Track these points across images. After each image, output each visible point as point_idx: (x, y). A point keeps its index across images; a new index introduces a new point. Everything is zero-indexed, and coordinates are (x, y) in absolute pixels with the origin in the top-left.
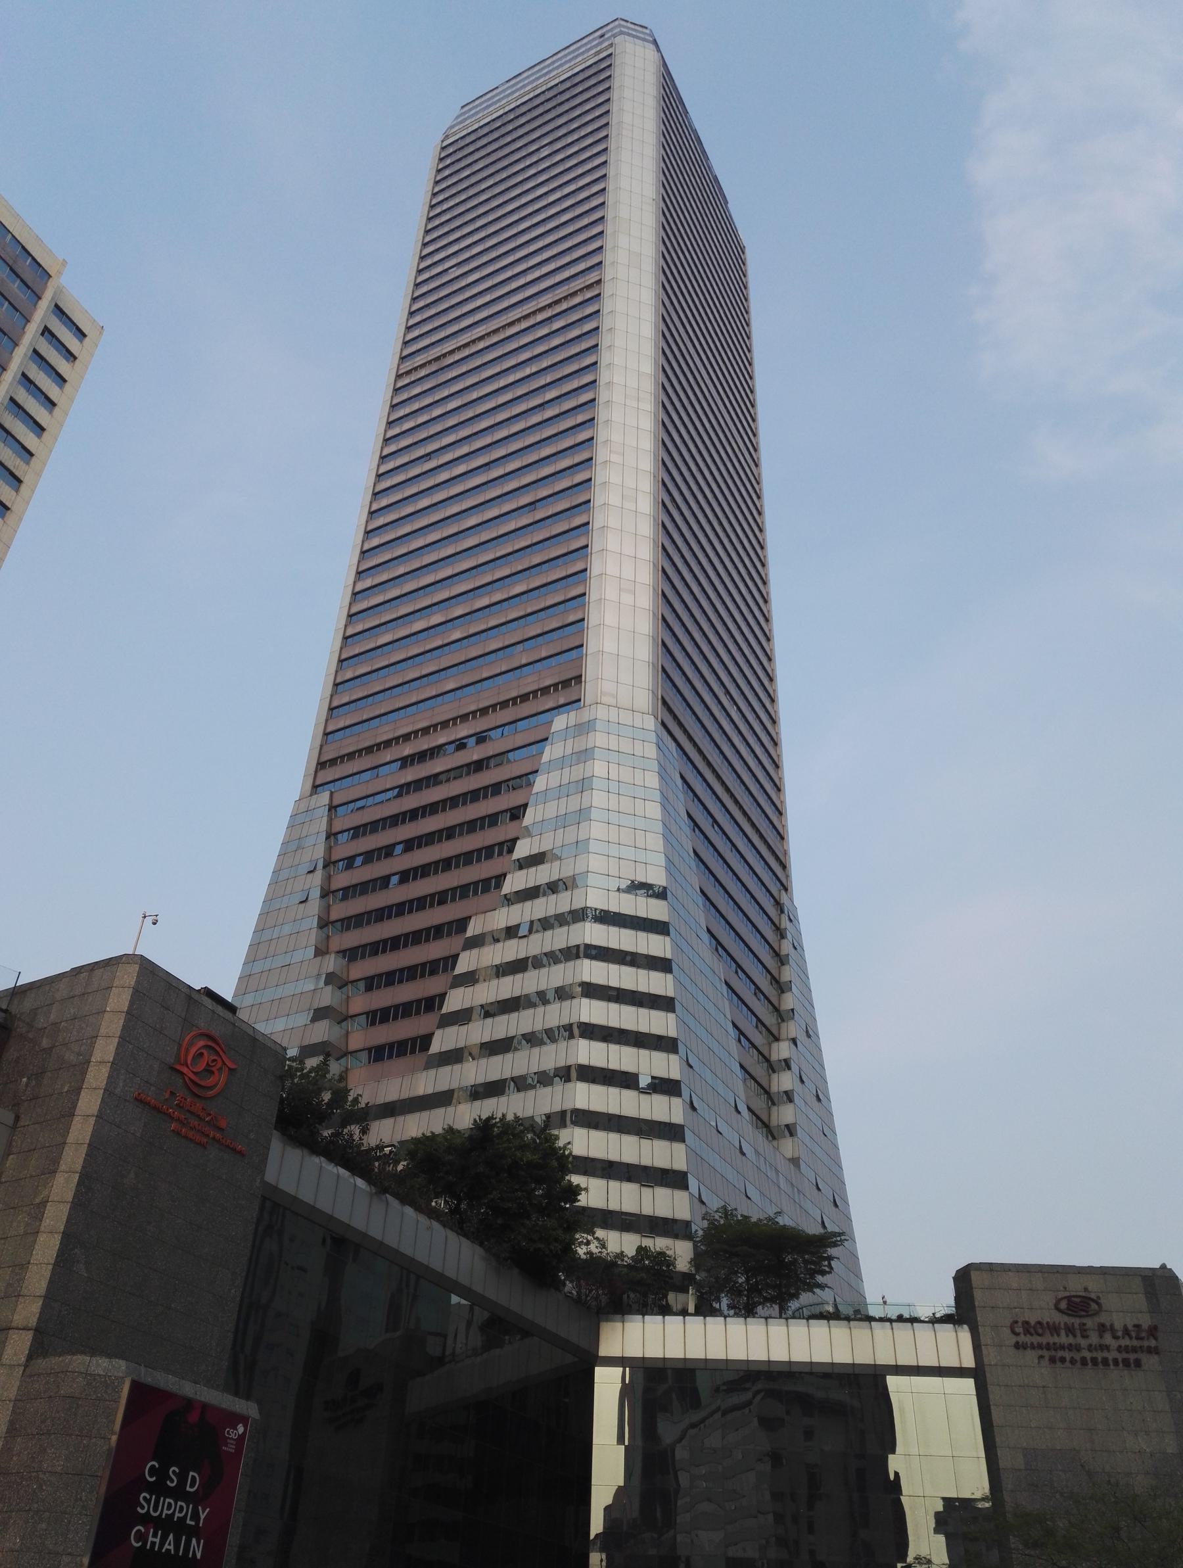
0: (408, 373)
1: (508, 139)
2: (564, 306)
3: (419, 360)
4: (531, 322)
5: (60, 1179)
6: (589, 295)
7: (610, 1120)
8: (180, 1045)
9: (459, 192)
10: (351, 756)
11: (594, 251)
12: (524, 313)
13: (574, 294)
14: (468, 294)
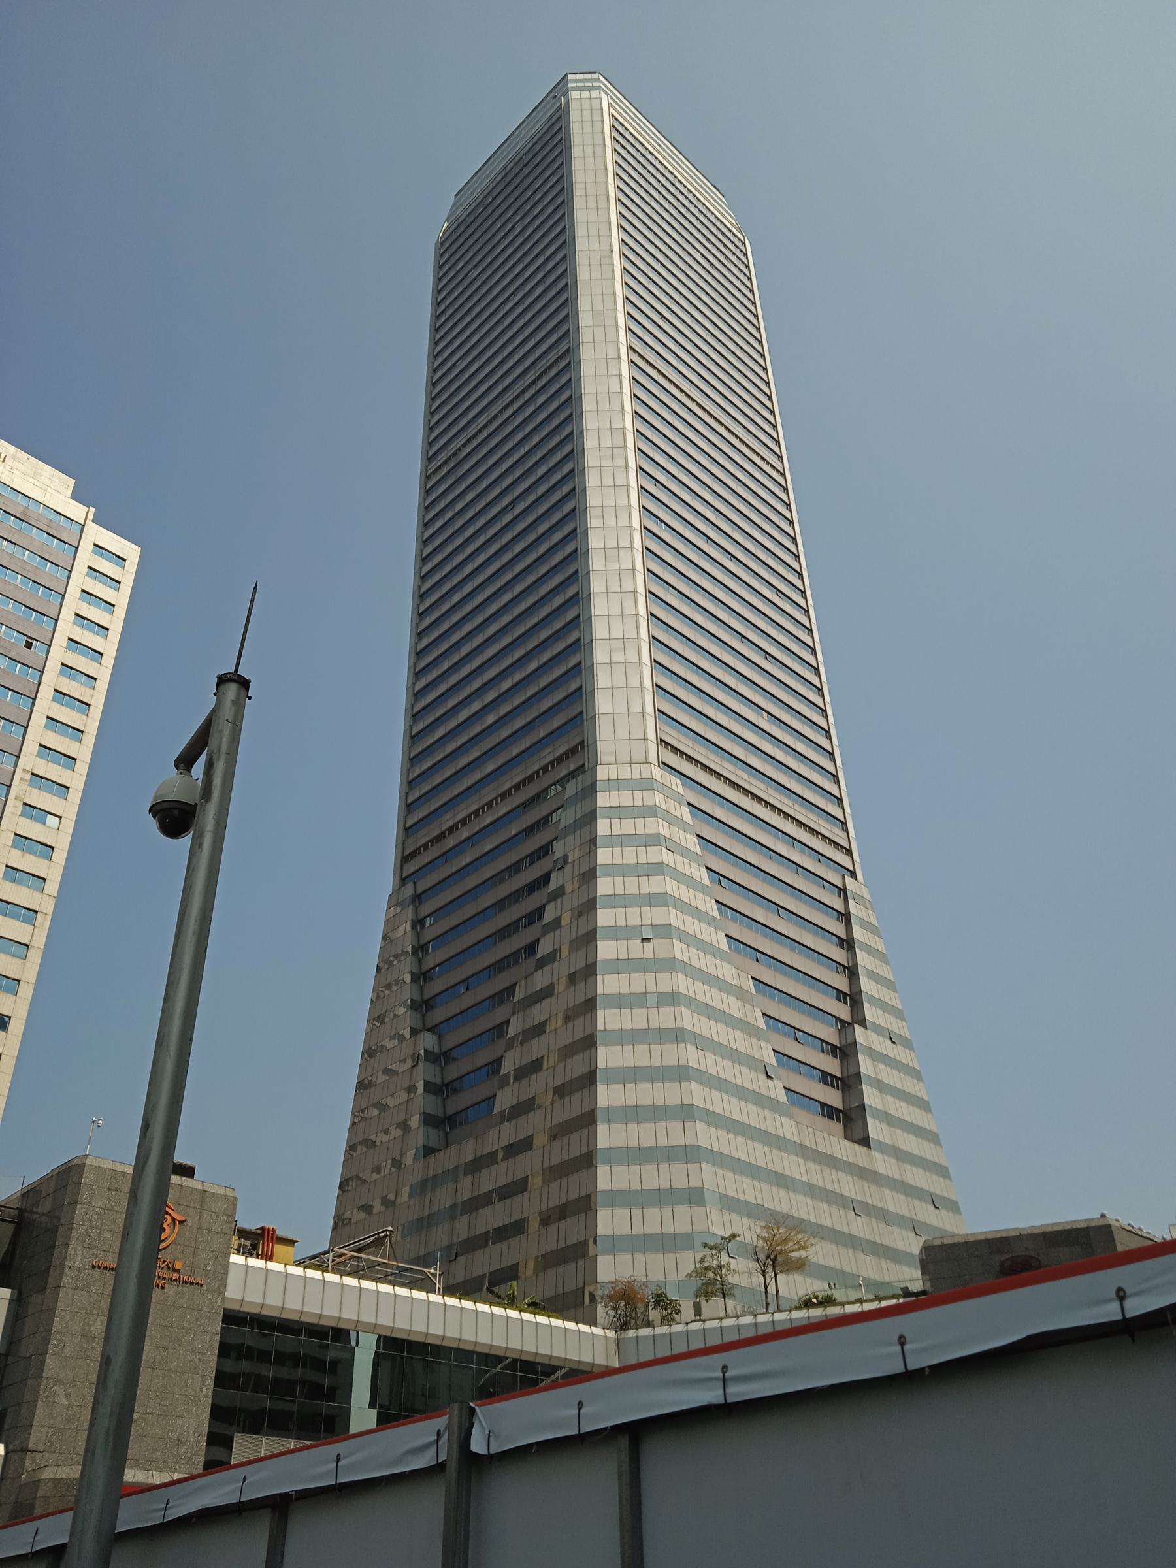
0: (434, 473)
3: (442, 458)
10: (425, 846)
13: (552, 366)
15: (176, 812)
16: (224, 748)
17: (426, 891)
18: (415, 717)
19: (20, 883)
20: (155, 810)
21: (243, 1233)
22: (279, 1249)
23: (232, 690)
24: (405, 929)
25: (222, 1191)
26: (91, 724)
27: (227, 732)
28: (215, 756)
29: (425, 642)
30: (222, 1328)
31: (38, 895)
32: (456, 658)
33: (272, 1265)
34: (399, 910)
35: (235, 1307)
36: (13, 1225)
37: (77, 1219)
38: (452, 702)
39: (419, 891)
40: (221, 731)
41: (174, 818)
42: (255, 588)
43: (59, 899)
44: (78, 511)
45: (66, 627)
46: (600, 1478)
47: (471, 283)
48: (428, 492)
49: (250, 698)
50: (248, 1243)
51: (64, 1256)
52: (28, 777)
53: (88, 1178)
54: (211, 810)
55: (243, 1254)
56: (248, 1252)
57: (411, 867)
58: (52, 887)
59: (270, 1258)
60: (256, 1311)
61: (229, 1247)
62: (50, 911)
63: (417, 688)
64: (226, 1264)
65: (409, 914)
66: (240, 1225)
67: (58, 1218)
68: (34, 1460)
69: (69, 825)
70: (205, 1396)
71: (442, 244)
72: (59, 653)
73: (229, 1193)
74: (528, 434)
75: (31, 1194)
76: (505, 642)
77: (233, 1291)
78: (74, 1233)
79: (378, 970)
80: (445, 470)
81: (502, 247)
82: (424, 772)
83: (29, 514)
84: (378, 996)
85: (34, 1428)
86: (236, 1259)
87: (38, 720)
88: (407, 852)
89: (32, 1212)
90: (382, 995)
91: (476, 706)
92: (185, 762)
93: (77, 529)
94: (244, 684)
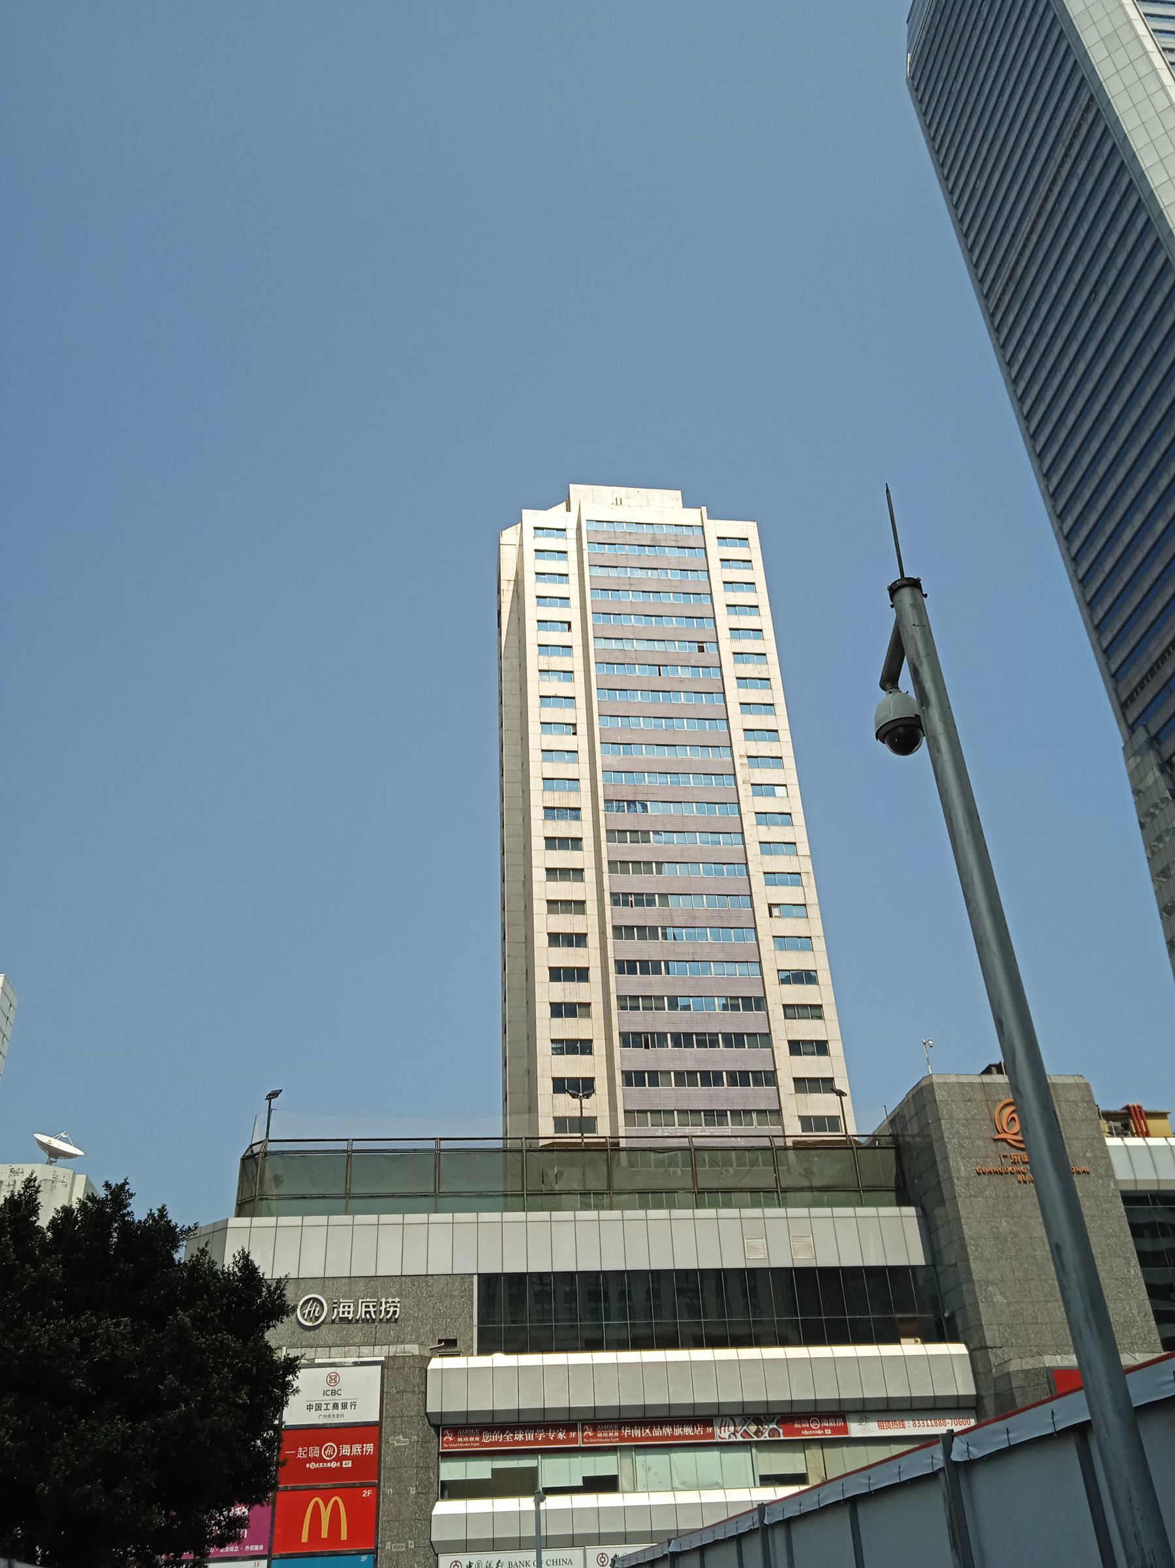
0: (997, 307)
1: (952, 23)
2: (1077, 145)
3: (999, 288)
4: (1060, 183)
5: (1031, 1361)
6: (1090, 118)
7: (594, 1296)
8: (993, 1121)
9: (944, 108)
10: (1141, 685)
11: (1072, 71)
12: (1051, 179)
13: (1079, 126)
14: (1000, 199)
15: (901, 730)
16: (922, 652)
17: (1160, 731)
18: (1075, 560)
19: (776, 854)
20: (881, 735)
21: (1109, 1116)
22: (1151, 1123)
23: (906, 594)
24: (1153, 776)
25: (1071, 1080)
26: (777, 695)
27: (918, 636)
28: (917, 664)
29: (1055, 480)
30: (1126, 1210)
31: (794, 858)
32: (1095, 480)
33: (1151, 1141)
34: (1139, 759)
35: (1131, 1187)
36: (893, 1151)
37: (946, 1134)
38: (1109, 528)
39: (1153, 732)
40: (913, 637)
41: (902, 735)
42: (887, 491)
43: (813, 856)
44: (692, 516)
45: (725, 622)
46: (697, 1556)
47: (958, 96)
48: (998, 330)
49: (926, 596)
50: (1118, 1124)
51: (948, 1169)
52: (745, 760)
53: (940, 1095)
54: (934, 713)
55: (1118, 1135)
56: (1124, 1131)
57: (1134, 711)
58: (804, 848)
59: (1147, 1134)
60: (1154, 1187)
61: (1100, 1131)
62: (810, 869)
63: (1066, 530)
64: (1105, 1149)
65: (1152, 759)
66: (1105, 1107)
67: (930, 1136)
68: (997, 1356)
69: (795, 790)
70: (1136, 1277)
71: (913, 78)
72: (727, 646)
73: (1078, 1080)
74: (1082, 211)
75: (895, 1119)
76: (1143, 439)
77: (1123, 1173)
78: (949, 1147)
79: (1142, 825)
80: (1007, 299)
81: (975, 40)
82: (1108, 611)
83: (657, 537)
84: (1153, 852)
85: (985, 1327)
86: (1111, 1142)
87: (734, 709)
88: (1124, 696)
89: (904, 1136)
90: (1156, 850)
91: (1138, 520)
92: (890, 680)
93: (698, 532)
94: (915, 584)
